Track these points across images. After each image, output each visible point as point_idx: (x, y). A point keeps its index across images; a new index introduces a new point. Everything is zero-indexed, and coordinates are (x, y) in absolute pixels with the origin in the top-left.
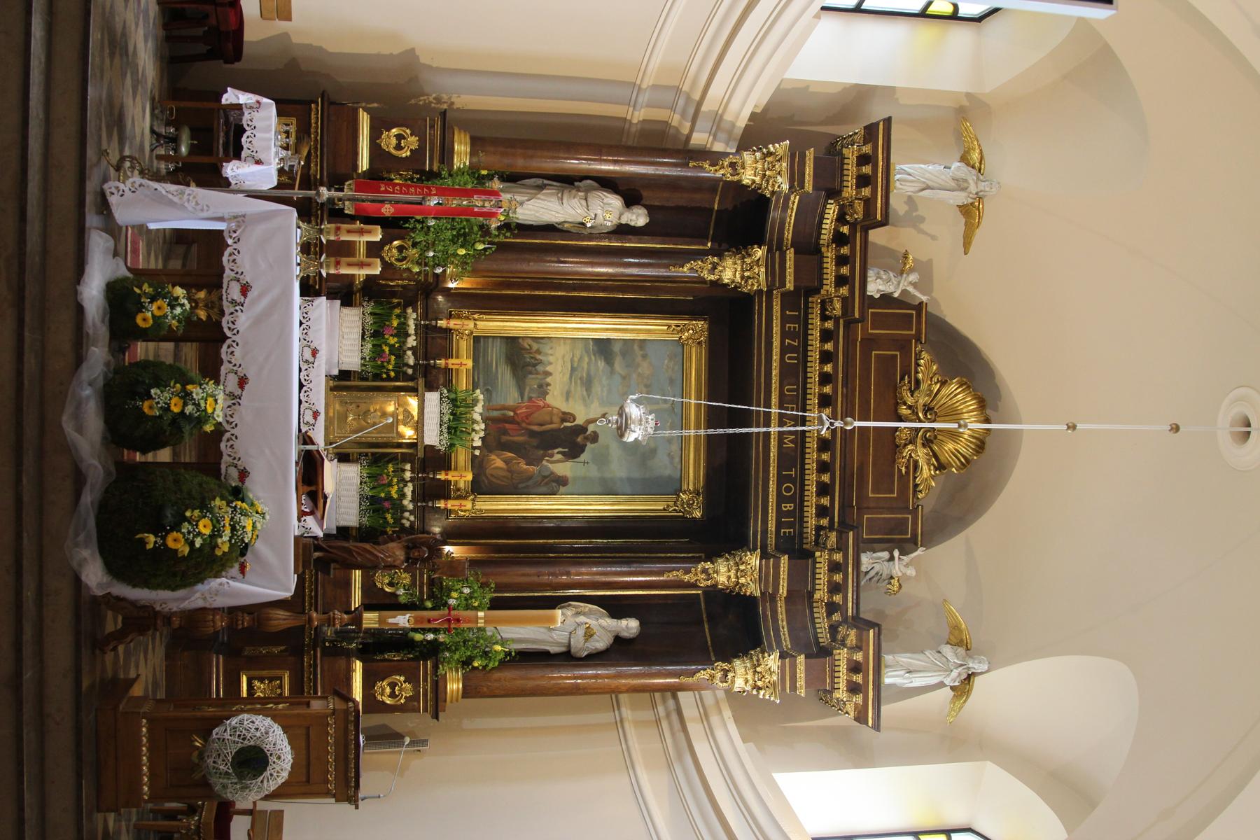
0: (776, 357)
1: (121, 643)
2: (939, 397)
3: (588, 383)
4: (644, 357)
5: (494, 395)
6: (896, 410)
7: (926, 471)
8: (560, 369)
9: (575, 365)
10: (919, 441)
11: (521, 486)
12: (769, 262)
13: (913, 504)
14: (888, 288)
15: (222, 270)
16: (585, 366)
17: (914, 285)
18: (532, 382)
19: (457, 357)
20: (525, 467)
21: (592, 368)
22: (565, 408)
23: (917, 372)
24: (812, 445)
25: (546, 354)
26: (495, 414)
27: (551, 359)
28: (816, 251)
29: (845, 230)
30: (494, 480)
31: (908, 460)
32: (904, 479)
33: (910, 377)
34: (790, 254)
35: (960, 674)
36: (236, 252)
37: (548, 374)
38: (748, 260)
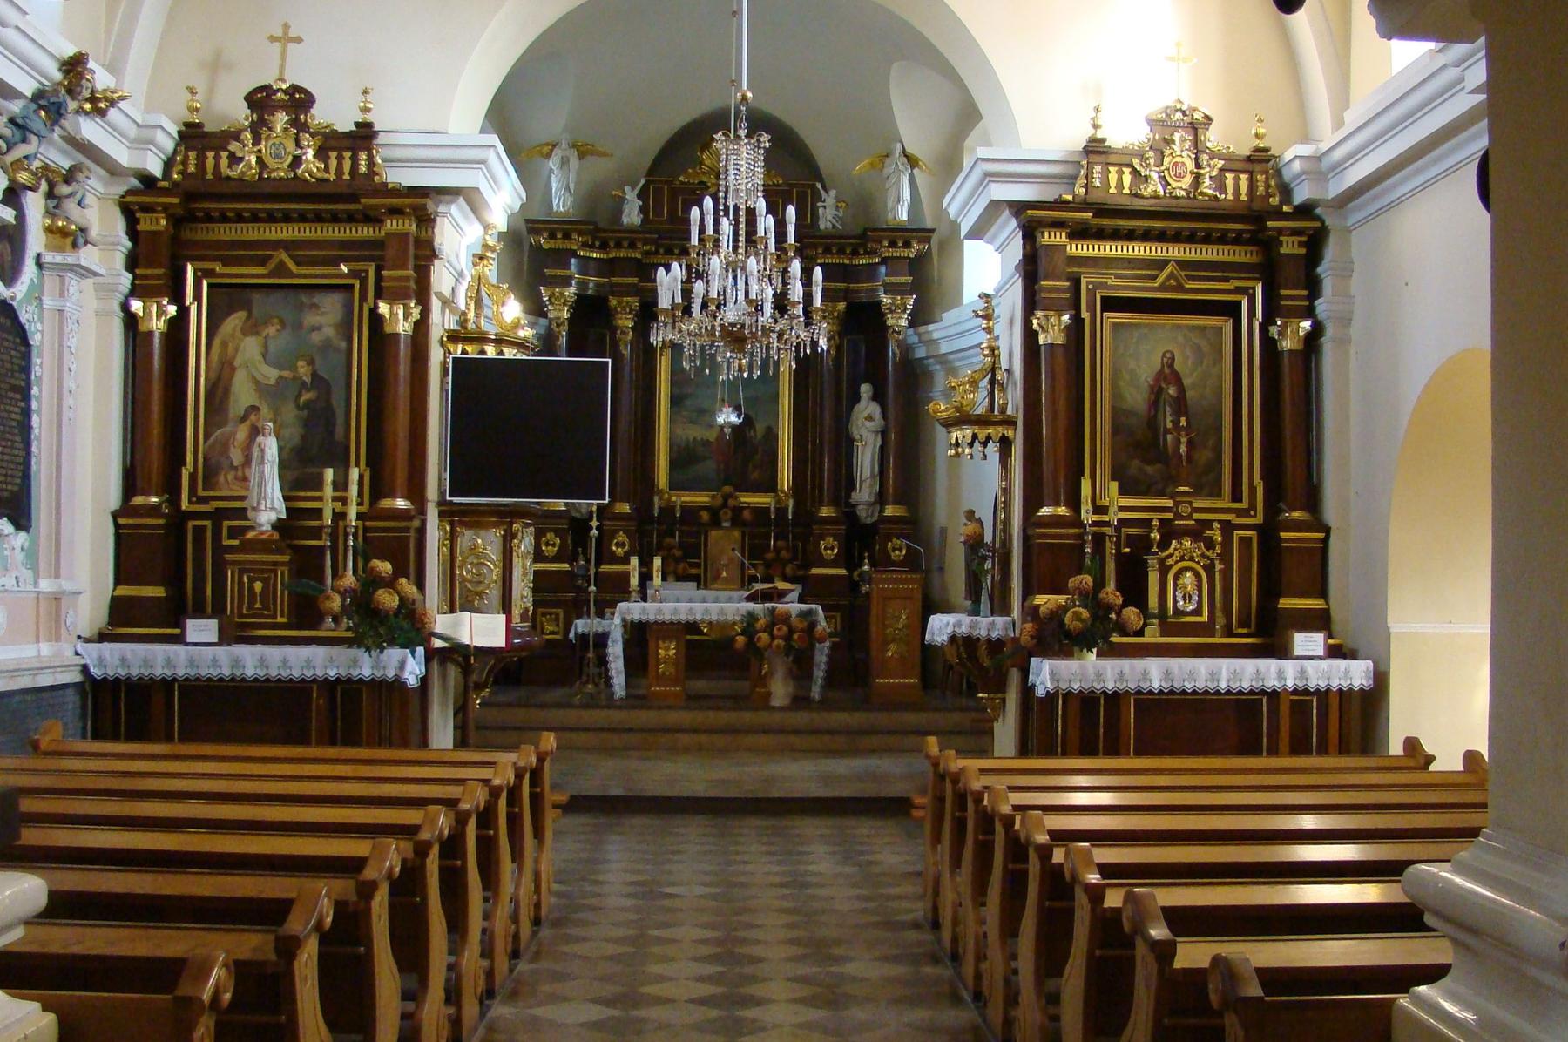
1: (1075, 878)
12: (621, 294)
14: (636, 210)
17: (633, 189)
27: (684, 438)
28: (612, 261)
29: (597, 244)
33: (697, 189)
34: (614, 280)
35: (903, 164)
37: (695, 439)
38: (619, 309)
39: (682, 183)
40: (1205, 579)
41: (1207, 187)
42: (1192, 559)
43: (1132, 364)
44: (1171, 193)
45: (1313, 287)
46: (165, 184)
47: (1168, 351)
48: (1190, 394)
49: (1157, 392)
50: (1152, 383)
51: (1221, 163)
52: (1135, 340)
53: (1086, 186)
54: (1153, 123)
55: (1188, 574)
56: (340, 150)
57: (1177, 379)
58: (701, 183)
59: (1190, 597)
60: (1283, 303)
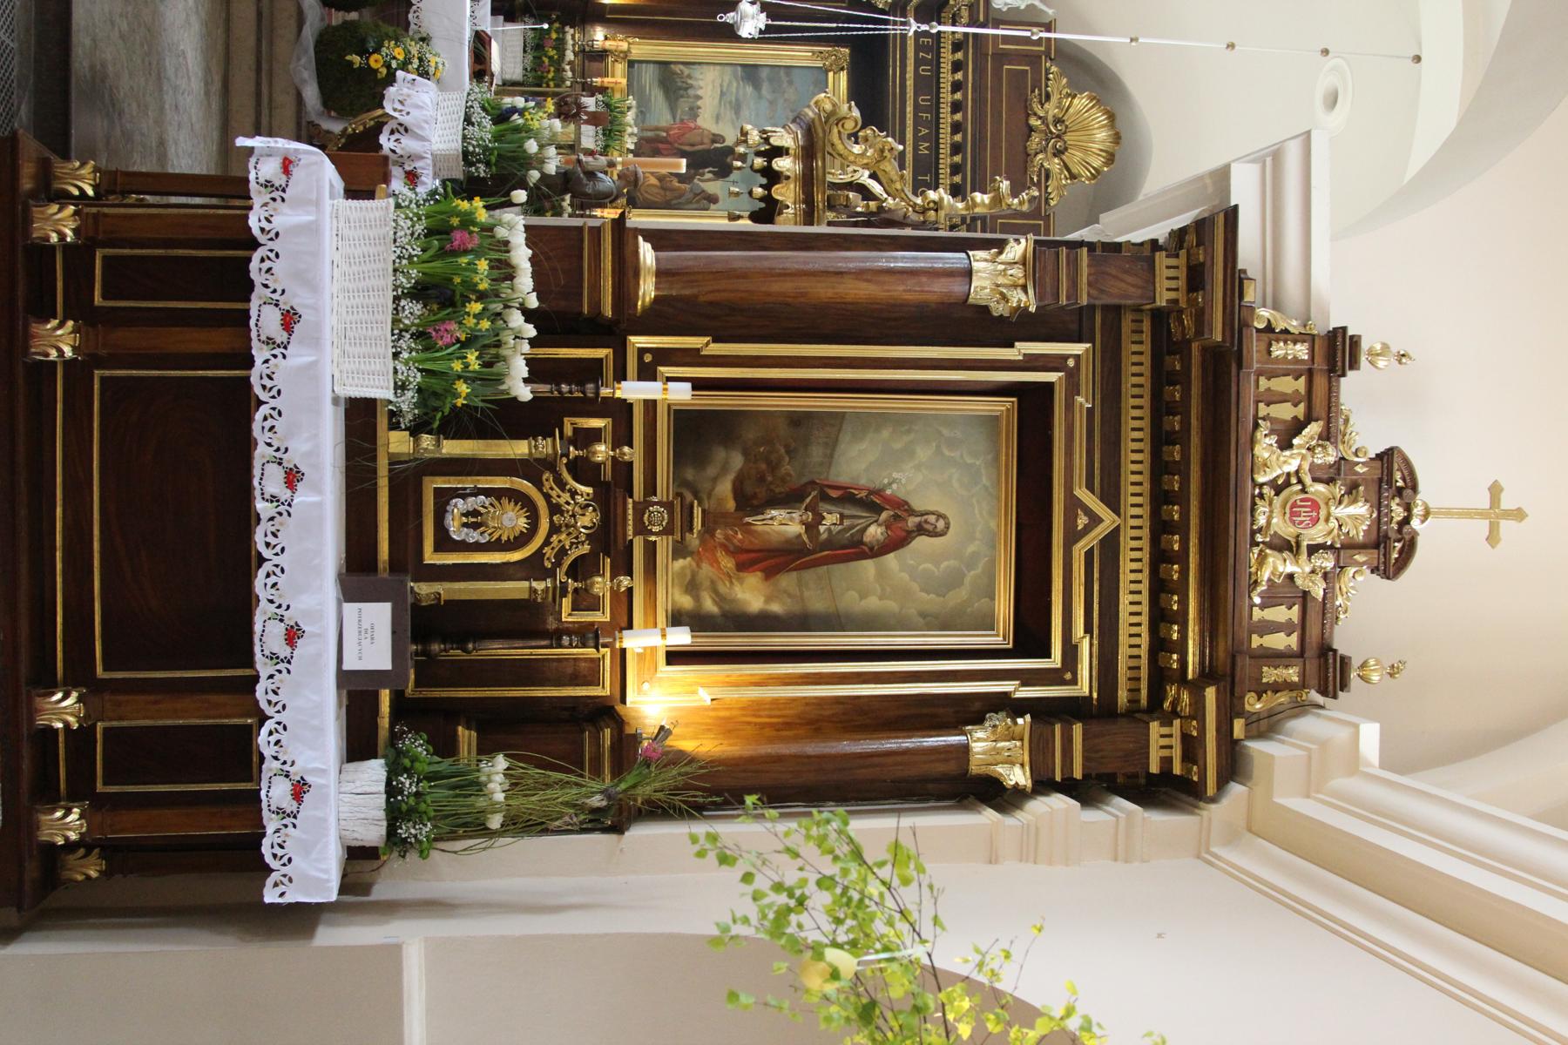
0: (910, 68)
2: (1071, 110)
3: (737, 108)
4: (790, 83)
5: (648, 115)
6: (1027, 120)
8: (709, 93)
9: (725, 90)
11: (674, 202)
16: (734, 90)
18: (684, 105)
19: (613, 76)
20: (677, 184)
21: (741, 93)
22: (715, 129)
25: (696, 79)
26: (650, 134)
30: (649, 197)
31: (1040, 170)
39: (1047, 72)
40: (516, 556)
41: (1277, 566)
42: (554, 529)
43: (923, 453)
44: (1261, 496)
45: (1086, 791)
47: (947, 527)
48: (868, 567)
49: (872, 502)
50: (888, 492)
51: (1318, 591)
52: (969, 461)
53: (1269, 329)
54: (1387, 457)
55: (522, 523)
57: (895, 543)
58: (1048, 97)
59: (475, 526)
60: (1058, 728)
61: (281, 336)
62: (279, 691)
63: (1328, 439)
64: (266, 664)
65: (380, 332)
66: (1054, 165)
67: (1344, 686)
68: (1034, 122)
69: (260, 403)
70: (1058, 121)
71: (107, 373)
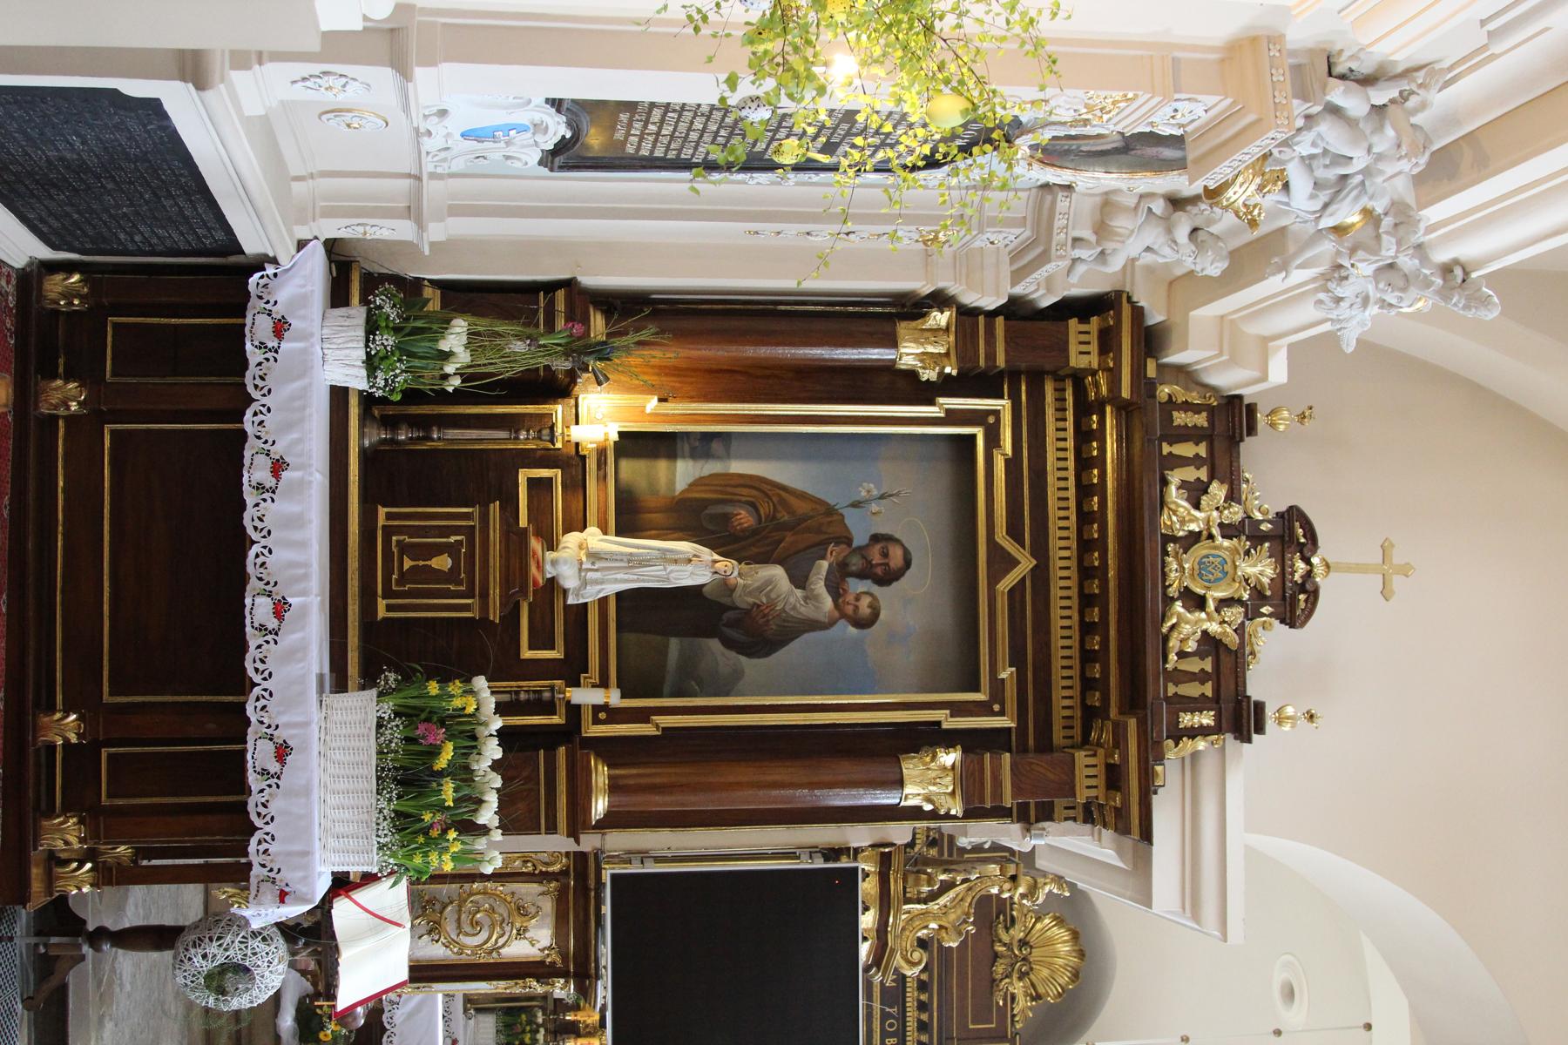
2: (1033, 932)
6: (993, 946)
7: (1022, 1003)
10: (1015, 976)
13: (1012, 1033)
15: (243, 579)
23: (1012, 909)
24: (911, 987)
31: (1006, 993)
32: (1002, 1011)
33: (1005, 916)
36: (266, 552)
46: (1151, 371)
56: (1216, 676)
61: (272, 623)
62: (264, 519)
63: (1232, 499)
64: (255, 635)
65: (366, 772)
66: (1018, 988)
67: (1260, 729)
68: (1000, 948)
69: (255, 685)
70: (1023, 943)
71: (115, 319)
